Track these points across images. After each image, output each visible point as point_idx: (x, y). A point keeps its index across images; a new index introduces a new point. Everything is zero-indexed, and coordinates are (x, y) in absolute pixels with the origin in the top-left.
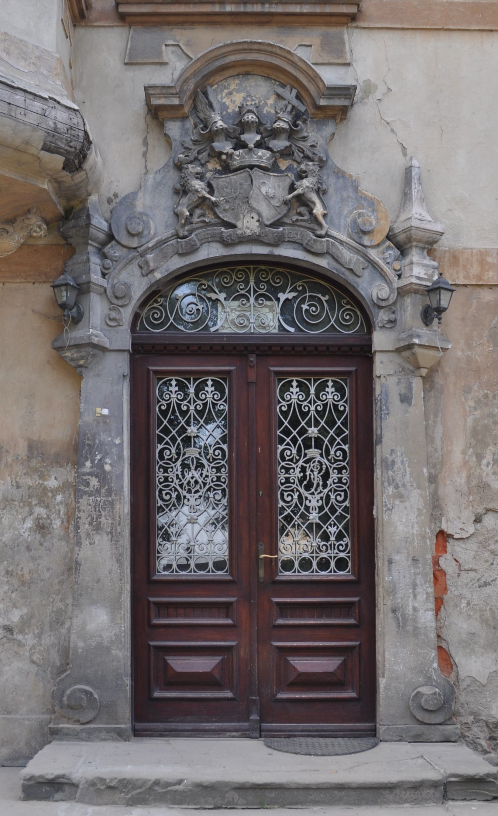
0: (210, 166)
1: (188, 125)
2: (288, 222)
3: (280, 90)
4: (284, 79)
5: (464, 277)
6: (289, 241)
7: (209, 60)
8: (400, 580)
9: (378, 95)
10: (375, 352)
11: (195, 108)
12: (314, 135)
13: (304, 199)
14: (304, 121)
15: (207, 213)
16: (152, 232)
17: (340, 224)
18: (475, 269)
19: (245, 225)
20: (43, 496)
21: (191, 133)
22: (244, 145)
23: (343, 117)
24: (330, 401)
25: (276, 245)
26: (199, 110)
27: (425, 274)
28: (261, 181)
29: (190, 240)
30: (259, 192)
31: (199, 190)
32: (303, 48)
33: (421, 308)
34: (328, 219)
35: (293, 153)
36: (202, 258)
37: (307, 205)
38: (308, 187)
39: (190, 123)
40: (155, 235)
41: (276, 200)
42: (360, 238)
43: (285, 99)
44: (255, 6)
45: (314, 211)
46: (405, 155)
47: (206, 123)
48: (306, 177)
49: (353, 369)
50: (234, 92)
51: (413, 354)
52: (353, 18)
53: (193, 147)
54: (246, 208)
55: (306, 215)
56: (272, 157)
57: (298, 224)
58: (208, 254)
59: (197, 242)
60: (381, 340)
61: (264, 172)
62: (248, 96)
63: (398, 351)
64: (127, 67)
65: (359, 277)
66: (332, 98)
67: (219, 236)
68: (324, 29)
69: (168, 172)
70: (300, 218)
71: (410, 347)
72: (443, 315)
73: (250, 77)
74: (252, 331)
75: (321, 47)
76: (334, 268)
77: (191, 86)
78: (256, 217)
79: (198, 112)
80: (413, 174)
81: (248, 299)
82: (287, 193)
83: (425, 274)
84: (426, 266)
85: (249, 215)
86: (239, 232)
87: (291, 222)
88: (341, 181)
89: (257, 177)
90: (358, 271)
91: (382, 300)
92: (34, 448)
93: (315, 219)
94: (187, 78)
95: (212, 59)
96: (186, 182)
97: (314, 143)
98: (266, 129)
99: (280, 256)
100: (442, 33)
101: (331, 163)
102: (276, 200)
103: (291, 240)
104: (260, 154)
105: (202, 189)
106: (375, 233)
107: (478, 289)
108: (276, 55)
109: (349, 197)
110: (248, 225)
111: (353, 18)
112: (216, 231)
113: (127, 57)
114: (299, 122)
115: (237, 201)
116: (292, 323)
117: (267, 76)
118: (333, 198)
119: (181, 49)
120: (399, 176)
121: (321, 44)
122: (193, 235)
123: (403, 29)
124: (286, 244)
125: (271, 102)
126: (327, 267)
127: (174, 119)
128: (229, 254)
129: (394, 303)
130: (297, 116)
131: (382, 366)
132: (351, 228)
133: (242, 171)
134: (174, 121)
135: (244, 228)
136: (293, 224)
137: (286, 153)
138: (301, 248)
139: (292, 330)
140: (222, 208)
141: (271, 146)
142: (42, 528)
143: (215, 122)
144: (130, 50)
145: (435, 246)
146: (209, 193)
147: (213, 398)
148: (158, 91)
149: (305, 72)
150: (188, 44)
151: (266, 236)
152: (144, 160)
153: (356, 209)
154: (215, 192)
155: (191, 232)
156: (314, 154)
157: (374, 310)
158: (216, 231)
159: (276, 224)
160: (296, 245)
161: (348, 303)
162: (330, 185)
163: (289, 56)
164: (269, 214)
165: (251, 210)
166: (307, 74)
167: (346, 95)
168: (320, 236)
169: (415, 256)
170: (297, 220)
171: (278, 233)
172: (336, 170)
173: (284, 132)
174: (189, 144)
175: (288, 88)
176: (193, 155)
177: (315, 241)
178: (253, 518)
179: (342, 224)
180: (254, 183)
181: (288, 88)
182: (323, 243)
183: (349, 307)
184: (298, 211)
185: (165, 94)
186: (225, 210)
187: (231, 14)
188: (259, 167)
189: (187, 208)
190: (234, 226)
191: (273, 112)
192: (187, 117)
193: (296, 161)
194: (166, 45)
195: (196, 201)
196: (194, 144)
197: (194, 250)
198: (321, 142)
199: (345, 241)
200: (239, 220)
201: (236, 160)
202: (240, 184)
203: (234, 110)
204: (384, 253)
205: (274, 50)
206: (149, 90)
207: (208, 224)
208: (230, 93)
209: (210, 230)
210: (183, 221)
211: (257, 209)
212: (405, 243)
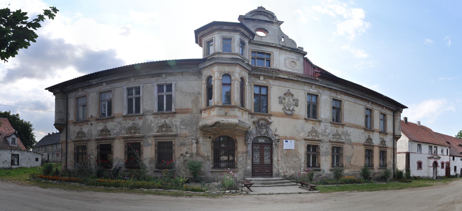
8: (275, 163)
12: (268, 126)
20: (243, 156)
45: (352, 141)
60: (274, 143)
92: (242, 152)
110: (263, 133)
131: (274, 146)
142: (243, 159)
178: (262, 158)
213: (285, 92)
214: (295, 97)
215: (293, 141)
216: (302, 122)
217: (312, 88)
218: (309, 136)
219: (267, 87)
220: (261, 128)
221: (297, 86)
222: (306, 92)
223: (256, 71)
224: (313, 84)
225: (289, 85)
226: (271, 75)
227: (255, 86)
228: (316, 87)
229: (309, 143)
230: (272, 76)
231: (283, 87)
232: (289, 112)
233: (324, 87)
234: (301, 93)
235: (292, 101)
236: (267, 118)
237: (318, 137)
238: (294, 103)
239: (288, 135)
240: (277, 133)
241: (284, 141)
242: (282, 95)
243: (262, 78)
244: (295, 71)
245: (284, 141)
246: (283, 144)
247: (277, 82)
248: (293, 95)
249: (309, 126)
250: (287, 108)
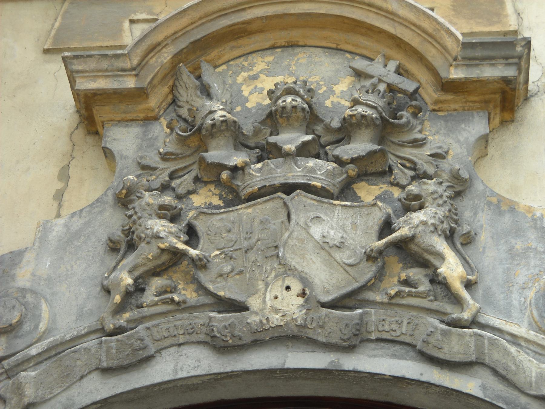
1: (157, 131)
2: (378, 298)
3: (360, 64)
4: (367, 44)
7: (207, 16)
13: (413, 247)
15: (180, 287)
16: (42, 326)
17: (510, 304)
19: (269, 303)
23: (507, 116)
25: (348, 348)
26: (180, 104)
29: (128, 337)
30: (304, 235)
31: (162, 234)
34: (480, 291)
35: (391, 170)
36: (158, 379)
37: (425, 264)
39: (160, 129)
40: (47, 332)
41: (348, 253)
43: (372, 77)
48: (421, 207)
50: (261, 75)
53: (162, 165)
54: (273, 269)
55: (423, 283)
57: (404, 302)
58: (175, 371)
59: (148, 341)
61: (318, 198)
64: (48, 57)
66: (477, 65)
67: (204, 329)
69: (100, 212)
70: (407, 289)
75: (454, 10)
76: (499, 397)
79: (180, 107)
82: (374, 235)
85: (280, 283)
86: (253, 319)
87: (385, 299)
88: (507, 219)
89: (301, 207)
94: (159, 44)
95: (214, 13)
96: (134, 222)
101: (481, 187)
102: (348, 253)
103: (386, 336)
105: (170, 233)
110: (277, 302)
112: (197, 321)
113: (50, 41)
115: (252, 256)
117: (334, 46)
118: (490, 254)
121: (453, 6)
124: (372, 345)
126: (479, 394)
128: (229, 369)
132: (537, 308)
133: (267, 198)
134: (127, 126)
135: (266, 311)
136: (392, 302)
138: (412, 353)
140: (214, 271)
143: (211, 112)
144: (59, 30)
146: (186, 243)
148: (92, 65)
149: (414, 25)
151: (321, 327)
152: (56, 205)
154: (202, 241)
158: (197, 321)
160: (398, 347)
162: (482, 227)
164: (327, 281)
165: (285, 273)
166: (419, 27)
167: (507, 58)
168: (457, 324)
170: (398, 294)
171: (352, 318)
172: (494, 200)
173: (367, 126)
174: (153, 159)
175: (380, 59)
177: (444, 333)
179: (515, 303)
180: (293, 217)
182: (467, 338)
184: (403, 276)
185: (107, 71)
186: (221, 275)
188: (307, 188)
189: (130, 272)
192: (156, 118)
193: (398, 185)
194: (132, 22)
195: (155, 258)
199: (525, 336)
200: (256, 293)
206: (72, 64)
207: (181, 307)
208: (255, 78)
209: (183, 320)
211: (300, 269)
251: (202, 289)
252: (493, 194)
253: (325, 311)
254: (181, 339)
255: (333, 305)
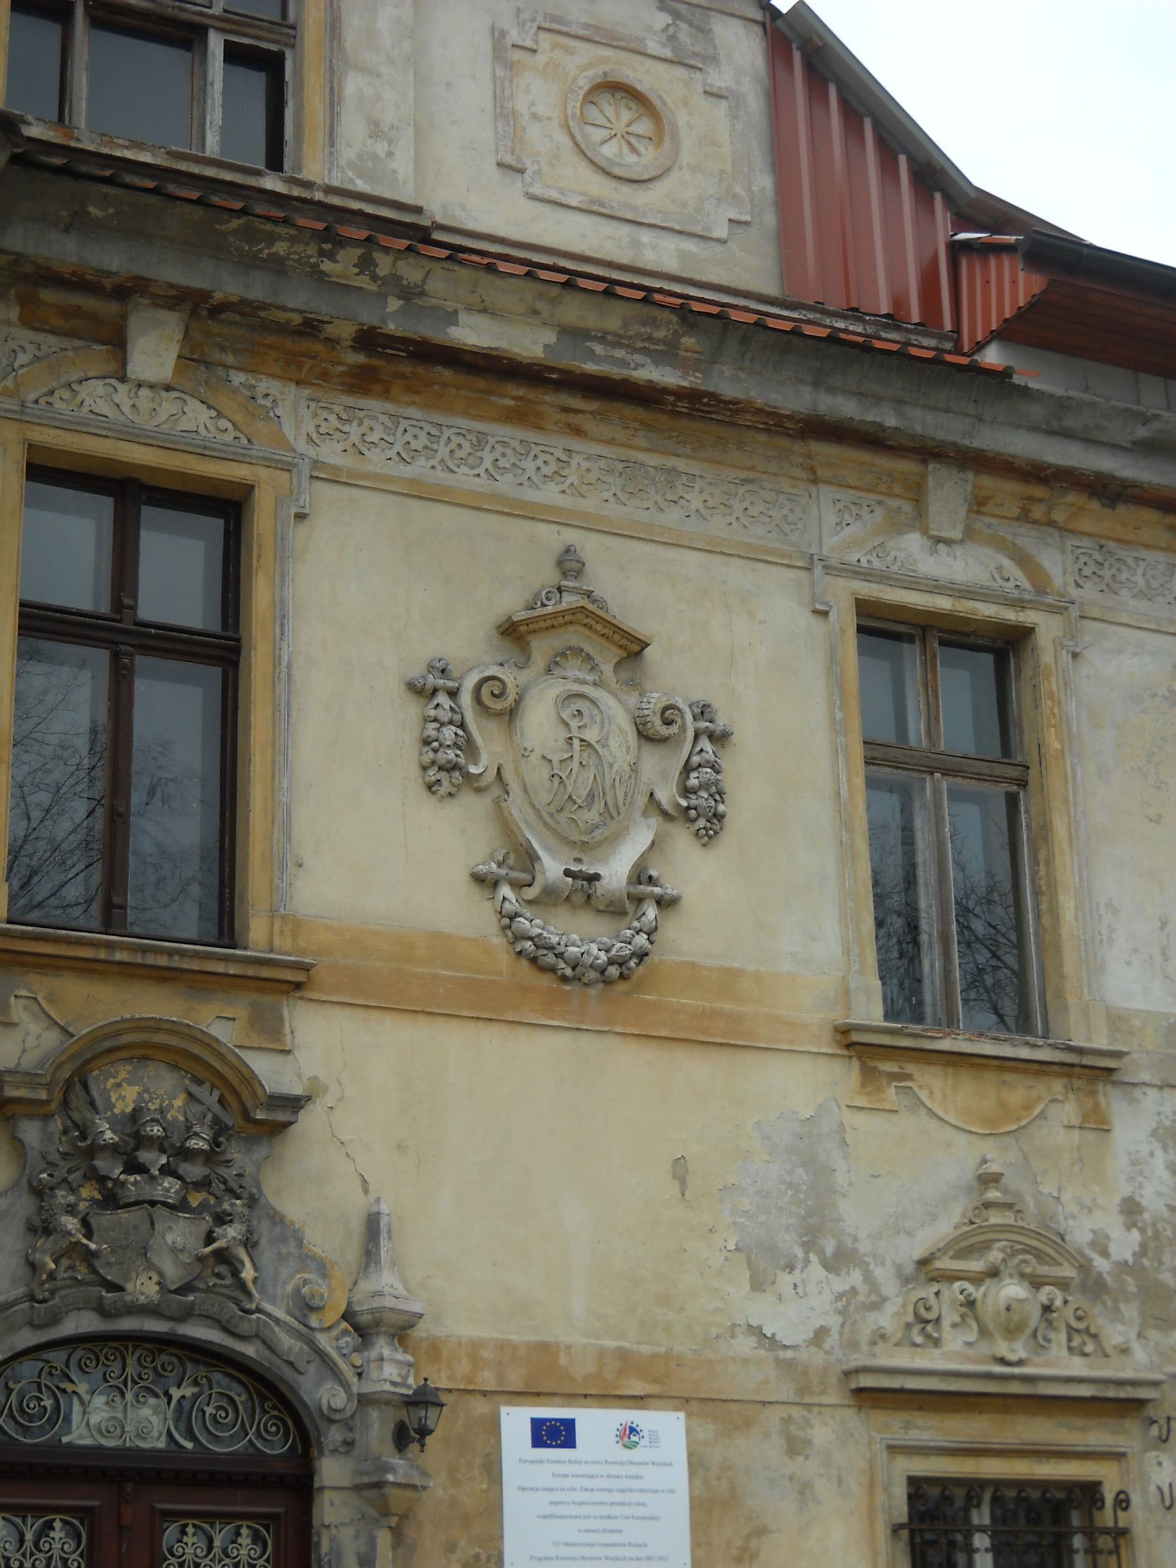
0: (85, 1193)
2: (201, 1286)
3: (195, 1089)
4: (200, 1072)
5: (450, 1379)
6: (200, 1315)
9: (329, 1100)
10: (322, 1489)
11: (65, 1103)
12: (234, 1152)
14: (228, 1139)
18: (464, 1367)
21: (56, 1138)
22: (142, 1169)
24: (244, 1559)
25: (181, 1319)
27: (399, 1375)
28: (167, 1225)
32: (223, 1021)
33: (392, 1426)
38: (234, 1238)
42: (305, 1316)
44: (159, 956)
46: (366, 1191)
47: (86, 1129)
48: (231, 1221)
49: (280, 1510)
51: (382, 1495)
52: (298, 986)
53: (62, 1163)
56: (182, 1189)
58: (77, 1328)
60: (331, 1471)
62: (144, 1091)
63: (358, 1488)
65: (301, 1373)
68: (254, 996)
70: (219, 1282)
71: (379, 1485)
72: (428, 1439)
73: (149, 1062)
74: (128, 1445)
77: (66, 1073)
78: (155, 1278)
80: (382, 1224)
81: (123, 1395)
82: (202, 1243)
83: (399, 1375)
84: (400, 1363)
86: (128, 1298)
88: (278, 1229)
90: (301, 1365)
91: (335, 1411)
93: (242, 1286)
97: (241, 1171)
98: (172, 1146)
99: (185, 1336)
100: (421, 1018)
104: (166, 1184)
106: (326, 1309)
107: (468, 1397)
108: (195, 1039)
109: (289, 1253)
110: (144, 1288)
111: (298, 986)
114: (222, 1139)
116: (192, 1437)
118: (267, 1255)
119: (39, 1004)
120: (357, 1224)
122: (57, 1299)
123: (366, 1006)
125: (179, 1102)
126: (254, 1356)
127: (31, 1117)
129: (352, 1416)
130: (220, 1129)
131: (334, 1511)
136: (208, 1290)
137: (203, 1184)
139: (189, 1445)
141: (180, 1171)
145: (409, 1331)
146: (84, 1236)
147: (62, 1549)
150: (50, 999)
153: (298, 1272)
155: (53, 1292)
156: (241, 1187)
157: (322, 1425)
159: (184, 1289)
161: (274, 1408)
163: (214, 1044)
164: (173, 1273)
169: (382, 1347)
174: (54, 1157)
175: (207, 1086)
176: (60, 1173)
177: (241, 1318)
181: (207, 1086)
183: (275, 1413)
184: (216, 1270)
187: (121, 963)
188: (165, 1204)
190: (121, 1289)
191: (182, 1118)
196: (64, 1159)
197: (55, 1319)
198: (250, 1169)
201: (130, 1190)
202: (134, 1227)
203: (123, 1111)
204: (338, 1340)
205: (193, 1033)
208: (119, 1085)
210: (44, 1276)
212: (369, 1327)
213: (511, 602)
214: (675, 676)
215: (667, 1429)
216: (803, 1087)
217: (919, 519)
218: (925, 1324)
219: (228, 508)
220: (111, 1200)
221: (703, 495)
222: (842, 595)
223: (77, 223)
224: (929, 452)
225: (569, 476)
226: (298, 299)
227: (47, 471)
228: (978, 504)
229: (943, 1447)
230: (311, 327)
231: (476, 504)
232: (583, 936)
233: (1108, 491)
234: (749, 617)
235: (620, 745)
236: (221, 1023)
237: (1083, 1336)
238: (660, 774)
239: (575, 1320)
240: (388, 1287)
241: (516, 1422)
242: (468, 646)
243: (155, 349)
244: (662, 254)
245: (516, 1422)
246: (492, 1468)
247: (382, 434)
248: (632, 649)
249: (912, 1163)
250: (552, 867)
251: (94, 1271)
252: (272, 1208)
253: (172, 1295)
254: (81, 1306)
255: (175, 1292)
